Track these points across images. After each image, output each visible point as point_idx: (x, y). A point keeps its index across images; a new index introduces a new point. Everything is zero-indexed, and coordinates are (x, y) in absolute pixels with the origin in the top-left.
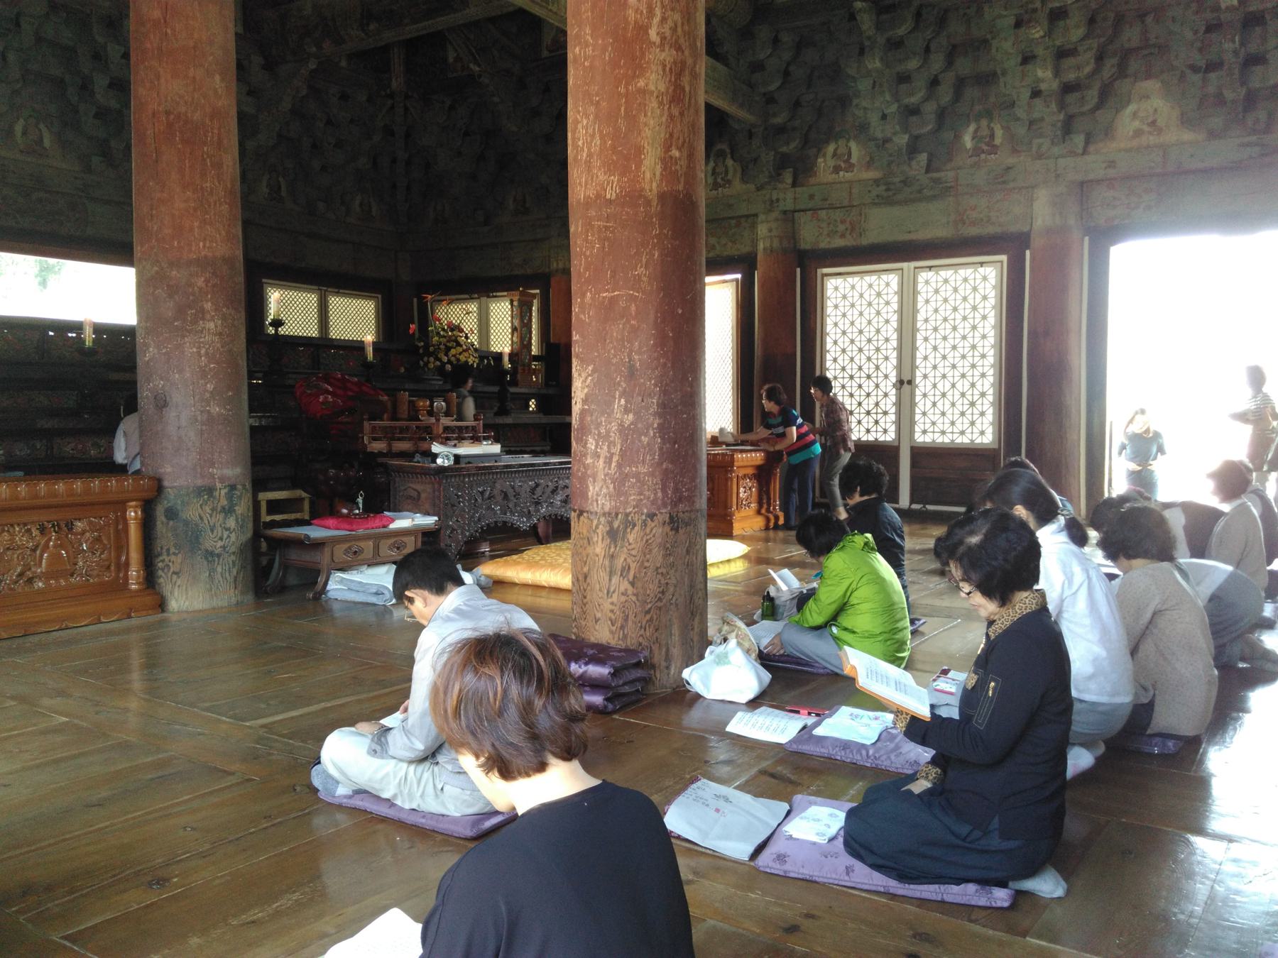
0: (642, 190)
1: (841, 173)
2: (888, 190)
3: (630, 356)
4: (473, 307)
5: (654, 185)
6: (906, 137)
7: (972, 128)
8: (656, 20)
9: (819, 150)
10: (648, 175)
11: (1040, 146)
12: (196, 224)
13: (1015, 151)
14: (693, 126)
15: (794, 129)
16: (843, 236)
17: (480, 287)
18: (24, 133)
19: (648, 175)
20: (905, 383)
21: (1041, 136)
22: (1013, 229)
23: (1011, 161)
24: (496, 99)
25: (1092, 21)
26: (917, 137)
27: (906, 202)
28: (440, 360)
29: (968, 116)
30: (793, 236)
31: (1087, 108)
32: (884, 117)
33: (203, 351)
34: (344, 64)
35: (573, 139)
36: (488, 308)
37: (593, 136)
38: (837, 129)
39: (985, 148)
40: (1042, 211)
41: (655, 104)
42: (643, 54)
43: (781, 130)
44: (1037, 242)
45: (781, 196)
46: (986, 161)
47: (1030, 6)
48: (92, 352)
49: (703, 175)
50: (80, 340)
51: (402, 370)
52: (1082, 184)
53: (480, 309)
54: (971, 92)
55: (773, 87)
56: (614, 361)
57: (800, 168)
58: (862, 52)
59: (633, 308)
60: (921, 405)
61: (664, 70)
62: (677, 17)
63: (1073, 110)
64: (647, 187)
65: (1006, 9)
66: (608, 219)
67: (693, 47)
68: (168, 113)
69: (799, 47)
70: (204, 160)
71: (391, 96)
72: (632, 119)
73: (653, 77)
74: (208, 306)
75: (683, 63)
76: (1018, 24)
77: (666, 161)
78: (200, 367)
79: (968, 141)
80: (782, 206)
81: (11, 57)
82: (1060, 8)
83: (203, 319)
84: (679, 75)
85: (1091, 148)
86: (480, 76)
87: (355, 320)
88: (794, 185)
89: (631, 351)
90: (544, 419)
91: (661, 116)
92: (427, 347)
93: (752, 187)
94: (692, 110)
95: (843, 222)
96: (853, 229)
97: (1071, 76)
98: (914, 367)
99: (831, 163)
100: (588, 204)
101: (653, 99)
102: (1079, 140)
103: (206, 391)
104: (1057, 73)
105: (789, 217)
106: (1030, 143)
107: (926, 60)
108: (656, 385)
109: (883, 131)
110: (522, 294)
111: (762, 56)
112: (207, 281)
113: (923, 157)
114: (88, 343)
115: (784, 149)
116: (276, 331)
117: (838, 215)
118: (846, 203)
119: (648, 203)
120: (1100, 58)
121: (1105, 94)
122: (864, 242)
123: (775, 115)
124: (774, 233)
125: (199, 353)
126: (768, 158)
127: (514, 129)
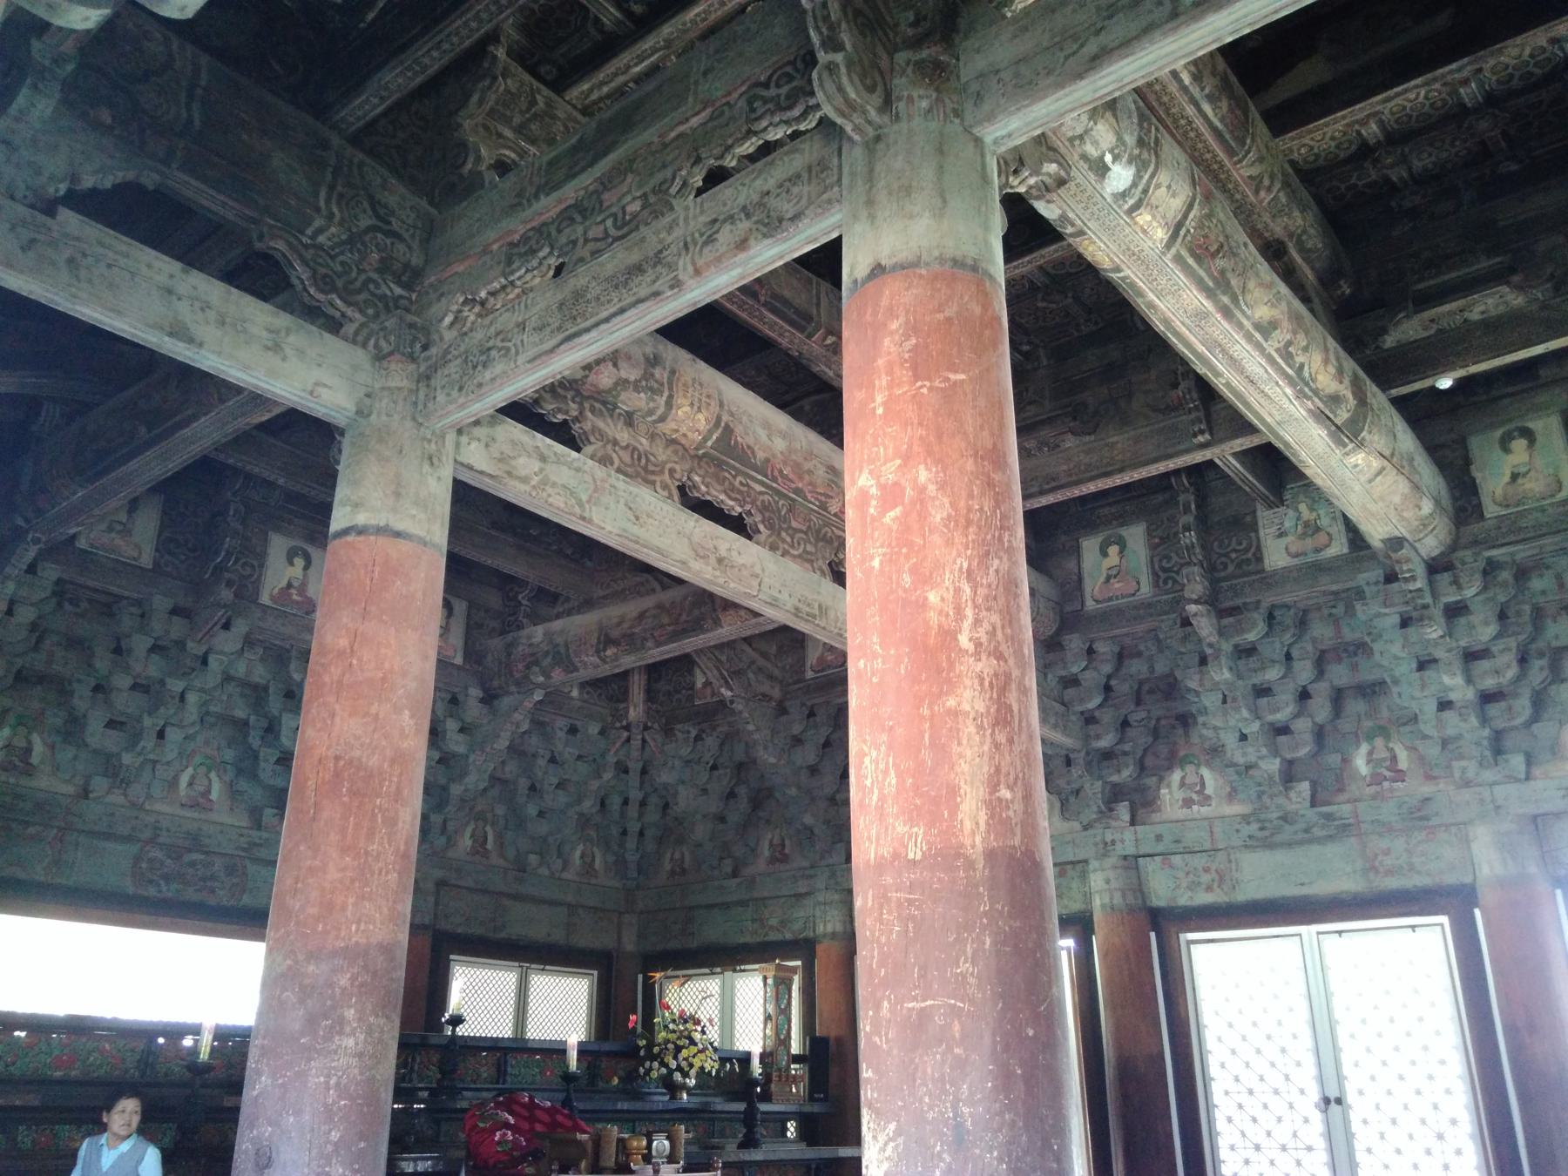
0: (962, 846)
1: (1195, 807)
2: (1262, 829)
3: (955, 1108)
4: (713, 985)
5: (978, 839)
6: (1278, 761)
7: (1364, 748)
8: (967, 624)
9: (1161, 779)
10: (968, 825)
11: (1464, 770)
12: (351, 900)
13: (1429, 778)
14: (1027, 756)
15: (1125, 754)
16: (1209, 889)
17: (724, 957)
18: (190, 784)
19: (968, 825)
20: (1332, 1102)
21: (1461, 757)
22: (1450, 879)
23: (1427, 789)
24: (751, 727)
25: (1502, 616)
26: (1291, 763)
27: (1289, 845)
28: (666, 1066)
29: (1357, 735)
30: (1139, 889)
31: (1518, 721)
32: (1243, 737)
33: (333, 1082)
34: (575, 693)
35: (859, 777)
36: (733, 987)
37: (886, 772)
38: (1182, 754)
39: (1388, 774)
40: (1486, 857)
41: (972, 729)
42: (951, 665)
43: (1107, 755)
44: (1486, 895)
45: (1117, 836)
46: (1391, 790)
47: (1420, 601)
48: (207, 1068)
49: (1046, 824)
50: (195, 1051)
51: (616, 1081)
52: (1535, 817)
53: (723, 988)
54: (1355, 706)
55: (1091, 705)
56: (930, 1116)
57: (1140, 802)
58: (1203, 661)
59: (957, 1027)
60: (1363, 1138)
61: (982, 684)
62: (996, 618)
63: (1500, 724)
64: (968, 842)
65: (1386, 606)
66: (911, 889)
67: (1019, 653)
68: (337, 758)
69: (1121, 657)
70: (374, 816)
71: (627, 728)
72: (941, 751)
73: (968, 694)
74: (350, 1013)
75: (1008, 676)
76: (1405, 623)
77: (994, 806)
78: (325, 1105)
79: (1361, 764)
80: (1119, 849)
81: (192, 698)
82: (1457, 602)
83: (341, 1033)
84: (1003, 690)
85: (1536, 771)
86: (732, 702)
87: (561, 1009)
88: (1133, 823)
89: (957, 1100)
90: (811, 1153)
91: (982, 743)
92: (650, 1046)
93: (1076, 825)
94: (1024, 737)
95: (1207, 870)
96: (1221, 879)
97: (1489, 683)
98: (1340, 1078)
99: (1179, 795)
100: (880, 866)
101: (969, 722)
102: (1517, 762)
103: (328, 1142)
104: (1469, 680)
105: (1131, 863)
106: (1449, 767)
107: (1289, 669)
108: (1000, 1160)
109: (1245, 754)
110: (802, 1077)
111: (1075, 669)
112: (353, 979)
113: (1305, 786)
114: (204, 1055)
115: (1115, 778)
116: (454, 1031)
117: (1199, 861)
118: (1207, 846)
119: (970, 865)
120: (1523, 660)
121: (1539, 702)
122: (1241, 896)
123: (1098, 737)
124: (1114, 884)
125: (327, 1083)
126: (1094, 789)
127: (772, 760)
